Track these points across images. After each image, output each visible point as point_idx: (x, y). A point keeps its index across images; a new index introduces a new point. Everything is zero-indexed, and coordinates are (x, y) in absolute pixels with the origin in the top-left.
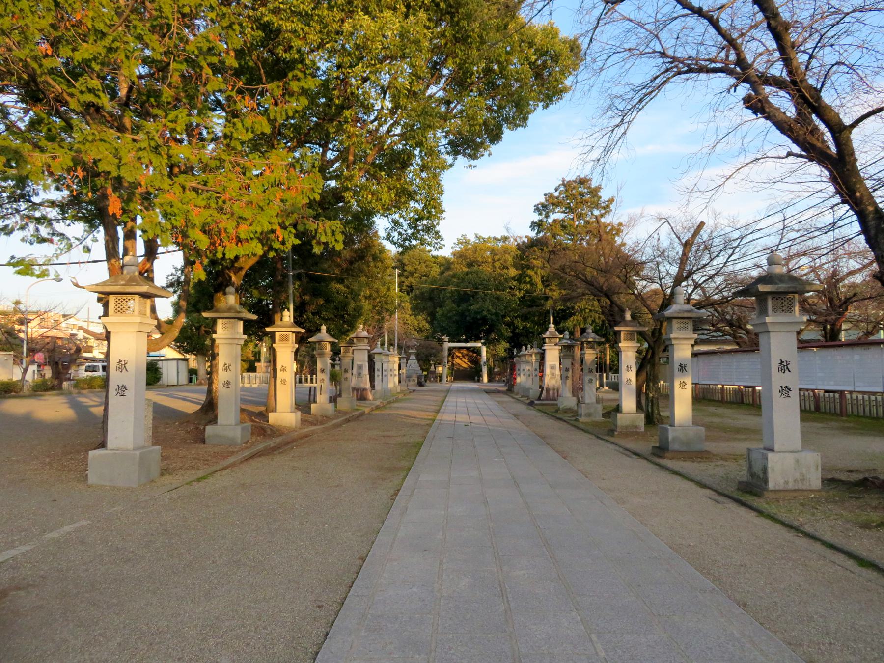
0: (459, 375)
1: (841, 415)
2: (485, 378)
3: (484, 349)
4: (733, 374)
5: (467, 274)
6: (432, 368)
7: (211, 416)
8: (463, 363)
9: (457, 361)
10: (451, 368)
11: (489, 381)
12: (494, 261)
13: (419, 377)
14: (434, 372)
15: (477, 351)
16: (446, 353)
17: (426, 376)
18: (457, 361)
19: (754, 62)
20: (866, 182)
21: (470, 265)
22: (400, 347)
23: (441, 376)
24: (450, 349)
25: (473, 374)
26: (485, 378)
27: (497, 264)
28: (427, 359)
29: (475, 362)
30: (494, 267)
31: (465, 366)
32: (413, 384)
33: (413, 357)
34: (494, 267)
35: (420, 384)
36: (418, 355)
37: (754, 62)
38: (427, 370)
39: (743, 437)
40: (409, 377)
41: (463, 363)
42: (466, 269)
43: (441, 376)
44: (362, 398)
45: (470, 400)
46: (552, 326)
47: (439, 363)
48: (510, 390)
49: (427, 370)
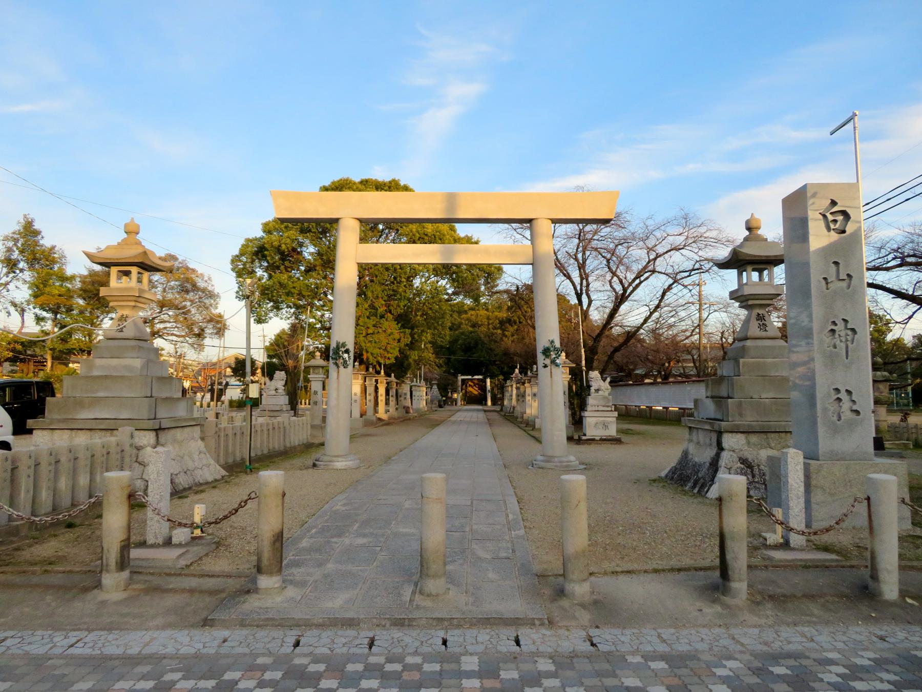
0: (470, 400)
1: (651, 418)
2: (489, 403)
3: (488, 381)
5: (471, 332)
6: (450, 394)
8: (475, 391)
9: (470, 389)
10: (465, 395)
11: (494, 403)
12: (489, 324)
13: (439, 401)
14: (451, 398)
16: (460, 383)
17: (444, 401)
18: (470, 389)
21: (474, 326)
22: (425, 380)
23: (456, 400)
24: (463, 380)
25: (480, 400)
26: (489, 403)
27: (491, 326)
28: (445, 388)
29: (483, 388)
30: (489, 329)
31: (476, 393)
32: (435, 407)
33: (435, 387)
34: (489, 329)
35: (440, 406)
36: (438, 385)
38: (446, 396)
40: (432, 401)
42: (470, 329)
43: (456, 400)
44: (407, 412)
45: (475, 414)
46: (517, 371)
49: (446, 396)
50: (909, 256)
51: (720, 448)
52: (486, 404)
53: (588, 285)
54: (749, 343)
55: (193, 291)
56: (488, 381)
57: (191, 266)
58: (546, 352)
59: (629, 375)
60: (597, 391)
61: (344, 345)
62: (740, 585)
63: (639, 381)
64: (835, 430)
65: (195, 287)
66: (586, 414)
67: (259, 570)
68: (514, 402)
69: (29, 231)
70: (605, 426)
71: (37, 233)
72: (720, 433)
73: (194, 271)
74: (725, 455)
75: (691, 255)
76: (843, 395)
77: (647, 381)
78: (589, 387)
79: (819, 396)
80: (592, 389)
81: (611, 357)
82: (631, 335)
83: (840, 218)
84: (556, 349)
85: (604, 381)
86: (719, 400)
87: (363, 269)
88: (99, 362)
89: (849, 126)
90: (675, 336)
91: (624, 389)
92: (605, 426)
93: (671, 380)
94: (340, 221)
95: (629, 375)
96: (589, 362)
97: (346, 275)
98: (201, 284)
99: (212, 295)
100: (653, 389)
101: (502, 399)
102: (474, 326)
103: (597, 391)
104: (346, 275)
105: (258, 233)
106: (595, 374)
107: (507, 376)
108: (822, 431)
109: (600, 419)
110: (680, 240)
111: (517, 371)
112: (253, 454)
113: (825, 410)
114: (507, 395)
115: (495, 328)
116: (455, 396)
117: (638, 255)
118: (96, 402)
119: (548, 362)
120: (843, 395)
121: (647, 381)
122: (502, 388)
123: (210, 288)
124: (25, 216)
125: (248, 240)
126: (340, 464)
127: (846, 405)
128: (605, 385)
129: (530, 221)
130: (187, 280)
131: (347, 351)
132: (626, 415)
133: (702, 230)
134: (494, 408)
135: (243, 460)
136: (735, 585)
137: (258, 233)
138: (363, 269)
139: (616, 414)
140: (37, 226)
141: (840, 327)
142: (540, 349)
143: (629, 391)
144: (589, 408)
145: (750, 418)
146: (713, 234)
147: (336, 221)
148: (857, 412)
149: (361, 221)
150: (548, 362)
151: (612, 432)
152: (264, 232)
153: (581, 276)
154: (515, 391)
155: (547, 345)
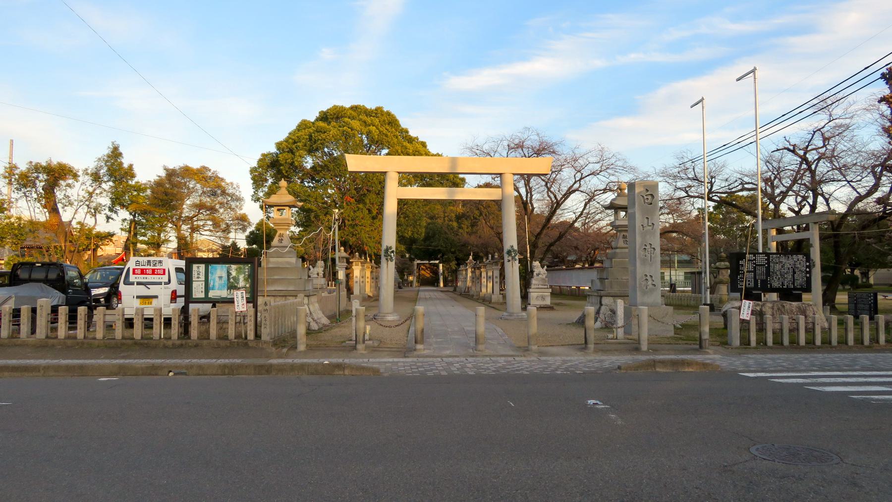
0: (424, 282)
2: (442, 285)
3: (441, 265)
4: (128, 333)
7: (494, 208)
8: (427, 274)
9: (423, 272)
10: (418, 277)
11: (445, 286)
15: (437, 266)
18: (423, 272)
19: (858, 193)
20: (576, 225)
25: (432, 282)
26: (442, 285)
29: (435, 272)
37: (858, 193)
39: (126, 354)
41: (427, 274)
43: (412, 282)
46: (471, 257)
47: (410, 274)
48: (455, 290)
50: (747, 183)
51: (601, 305)
52: (438, 286)
53: (532, 196)
54: (618, 251)
55: (222, 195)
56: (441, 265)
57: (220, 176)
58: (509, 252)
59: (563, 261)
60: (538, 275)
61: (391, 248)
62: (591, 346)
63: (571, 266)
64: (644, 293)
65: (224, 192)
66: (531, 290)
67: (416, 342)
68: (469, 284)
69: (115, 154)
70: (543, 298)
71: (121, 154)
72: (601, 297)
73: (222, 180)
74: (603, 308)
75: (604, 179)
76: (649, 278)
77: (577, 266)
78: (532, 272)
79: (638, 277)
80: (535, 274)
81: (548, 250)
82: (569, 226)
83: (650, 197)
84: (514, 251)
85: (543, 267)
86: (602, 280)
87: (402, 203)
88: (272, 260)
89: (700, 104)
90: (599, 229)
91: (558, 273)
92: (543, 298)
93: (597, 265)
94: (388, 174)
95: (563, 261)
96: (532, 253)
97: (391, 208)
98: (230, 191)
99: (239, 199)
100: (581, 273)
101: (456, 280)
102: (431, 218)
103: (538, 275)
104: (391, 208)
105: (273, 150)
106: (536, 264)
107: (461, 261)
108: (638, 293)
109: (539, 294)
110: (597, 167)
111: (471, 257)
112: (341, 309)
113: (640, 284)
114: (461, 277)
115: (451, 220)
116: (411, 278)
117: (567, 176)
118: (275, 281)
119: (510, 258)
120: (649, 278)
121: (577, 266)
122: (455, 272)
123: (237, 193)
124: (113, 143)
125: (263, 155)
126: (390, 318)
127: (650, 282)
128: (543, 271)
129: (501, 174)
130: (219, 187)
131: (393, 252)
132: (558, 293)
133: (613, 161)
134: (446, 289)
135: (335, 313)
136: (589, 346)
137: (273, 150)
138: (402, 203)
139: (550, 290)
140: (121, 150)
141: (648, 246)
142: (505, 251)
143: (562, 274)
144: (533, 286)
145: (616, 290)
146: (620, 163)
147: (385, 173)
148: (654, 285)
149: (399, 173)
150: (510, 258)
151: (548, 301)
152: (278, 149)
153: (527, 190)
154: (469, 274)
155: (509, 248)
